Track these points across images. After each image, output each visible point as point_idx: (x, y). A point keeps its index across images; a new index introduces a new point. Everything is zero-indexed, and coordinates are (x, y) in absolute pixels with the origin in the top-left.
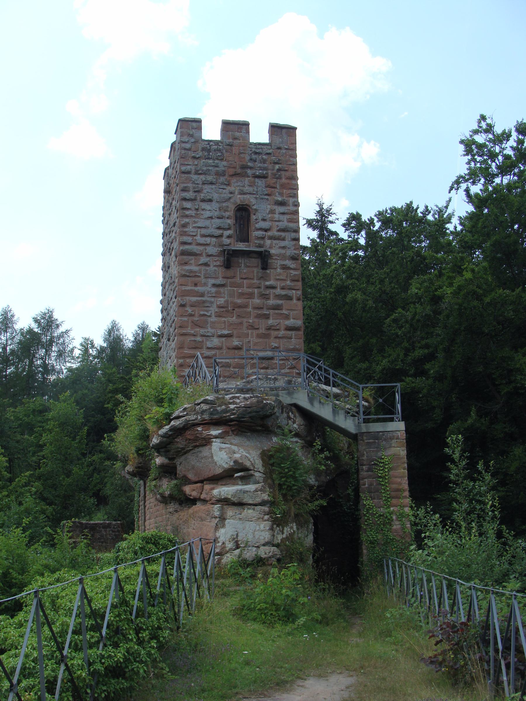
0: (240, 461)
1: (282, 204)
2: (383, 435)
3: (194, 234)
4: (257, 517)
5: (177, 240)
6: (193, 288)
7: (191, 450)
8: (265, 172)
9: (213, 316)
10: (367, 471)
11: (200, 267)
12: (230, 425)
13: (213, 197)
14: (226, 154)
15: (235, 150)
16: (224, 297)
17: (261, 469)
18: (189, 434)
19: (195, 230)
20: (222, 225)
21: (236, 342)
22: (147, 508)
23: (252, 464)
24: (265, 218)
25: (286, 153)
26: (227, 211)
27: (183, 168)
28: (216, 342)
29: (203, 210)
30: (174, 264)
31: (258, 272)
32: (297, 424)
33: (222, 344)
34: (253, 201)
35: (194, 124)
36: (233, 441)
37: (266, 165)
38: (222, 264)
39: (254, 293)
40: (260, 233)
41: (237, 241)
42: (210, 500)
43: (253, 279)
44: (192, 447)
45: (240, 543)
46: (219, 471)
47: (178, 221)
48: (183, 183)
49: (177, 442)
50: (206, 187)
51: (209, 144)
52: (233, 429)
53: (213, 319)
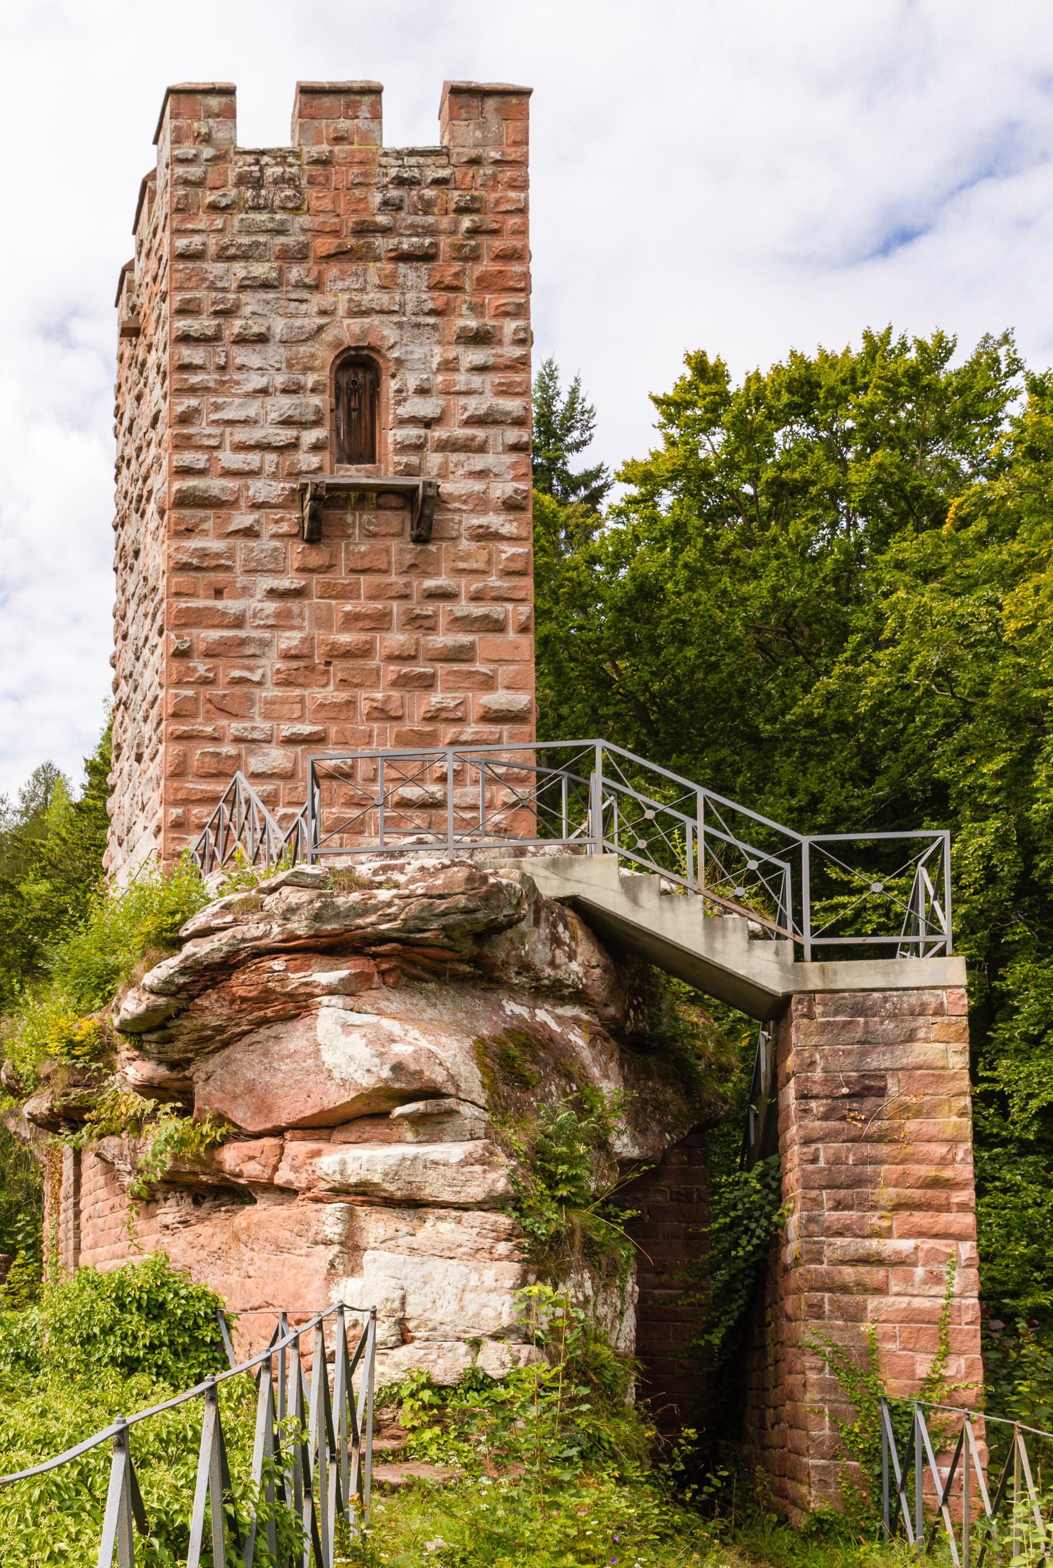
0: (413, 1067)
1: (480, 338)
2: (886, 1000)
3: (213, 442)
4: (470, 1244)
5: (165, 463)
6: (211, 603)
7: (245, 1033)
8: (427, 241)
9: (269, 684)
10: (825, 1117)
11: (231, 541)
12: (375, 956)
13: (269, 328)
14: (312, 194)
15: (339, 176)
16: (300, 628)
17: (481, 1097)
18: (242, 984)
19: (215, 431)
20: (296, 413)
21: (331, 758)
22: (84, 1216)
23: (451, 1077)
24: (426, 386)
25: (494, 176)
26: (311, 369)
27: (181, 243)
28: (276, 757)
29: (241, 368)
30: (155, 539)
31: (401, 551)
32: (580, 962)
33: (295, 763)
34: (391, 335)
35: (214, 103)
36: (383, 1004)
37: (431, 219)
38: (295, 530)
39: (390, 613)
40: (412, 433)
41: (339, 461)
42: (309, 1189)
43: (386, 572)
44: (250, 1022)
45: (411, 1325)
46: (336, 1097)
47: (164, 407)
48: (180, 289)
49: (203, 1009)
50: (246, 297)
51: (257, 162)
52: (385, 966)
53: (271, 692)
